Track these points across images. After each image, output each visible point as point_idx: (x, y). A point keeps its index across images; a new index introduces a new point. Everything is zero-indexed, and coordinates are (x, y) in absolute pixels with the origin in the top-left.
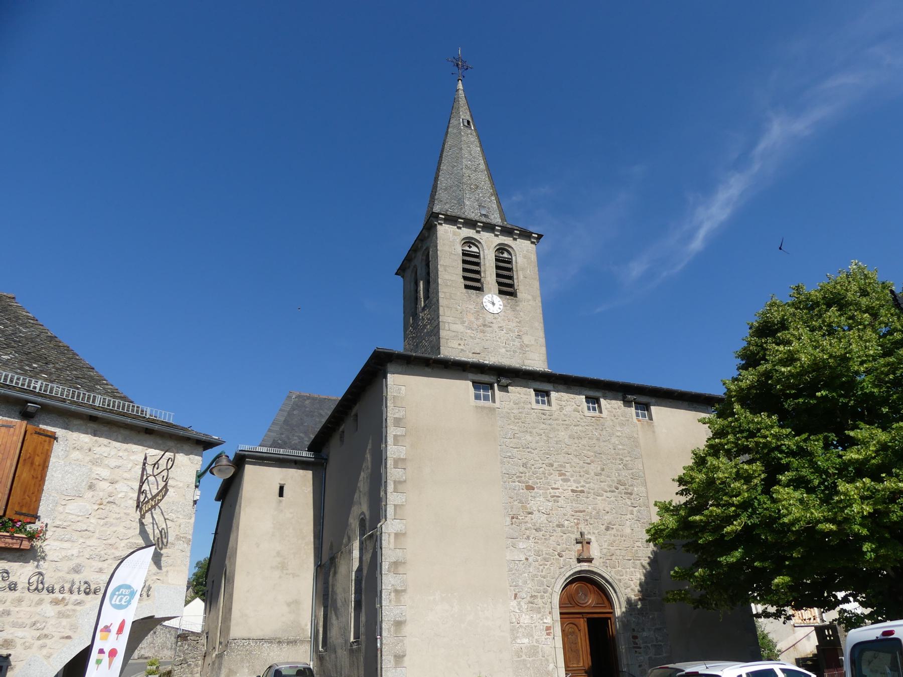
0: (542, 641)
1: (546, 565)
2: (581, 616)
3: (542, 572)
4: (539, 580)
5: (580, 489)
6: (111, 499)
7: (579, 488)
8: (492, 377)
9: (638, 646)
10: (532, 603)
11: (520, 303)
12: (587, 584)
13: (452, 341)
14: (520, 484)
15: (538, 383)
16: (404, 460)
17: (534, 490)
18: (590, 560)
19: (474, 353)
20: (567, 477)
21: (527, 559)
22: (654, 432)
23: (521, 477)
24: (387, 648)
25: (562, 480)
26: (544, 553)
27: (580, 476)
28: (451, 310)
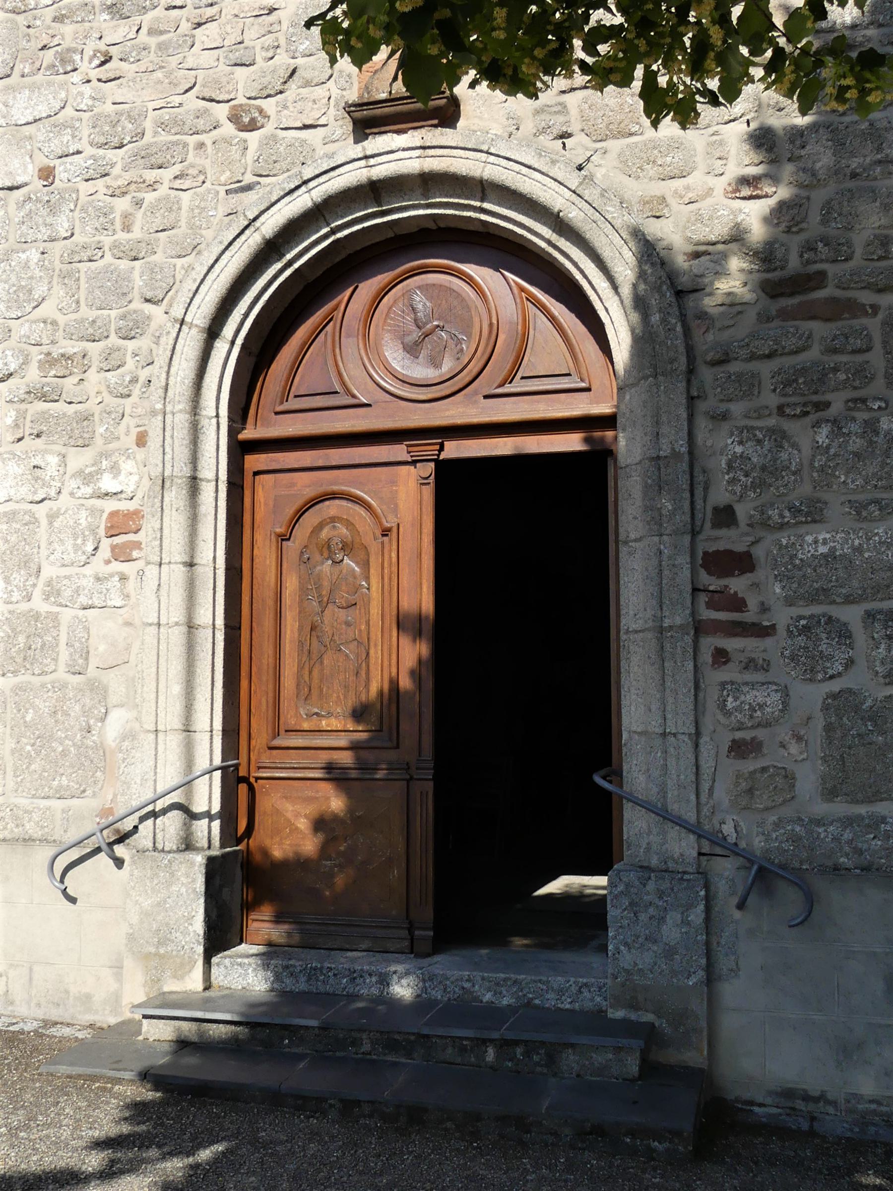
0: (77, 591)
1: (152, 186)
2: (399, 452)
3: (127, 228)
4: (107, 269)
9: (750, 616)
10: (44, 397)
12: (468, 269)
21: (47, 174)
26: (148, 124)
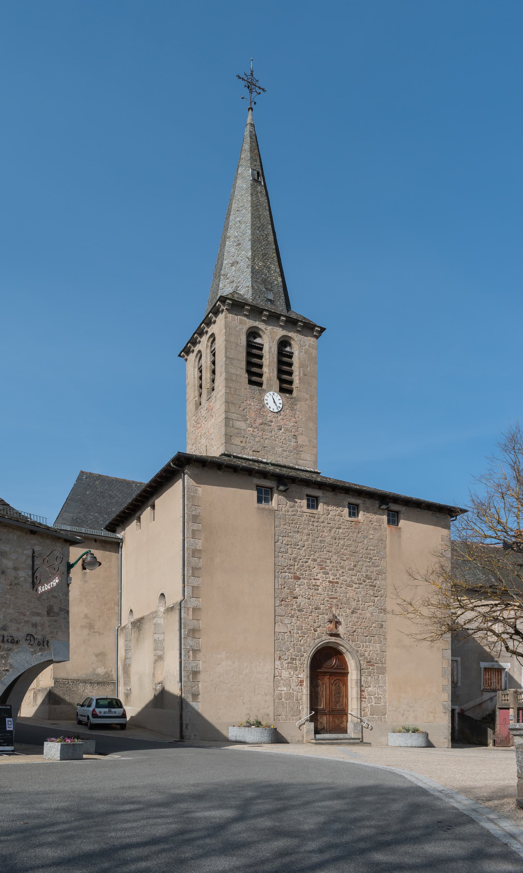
5: (335, 580)
6: (17, 582)
7: (335, 580)
9: (364, 697)
11: (299, 403)
13: (235, 438)
14: (289, 574)
15: (310, 489)
16: (200, 551)
17: (300, 579)
18: (337, 635)
19: (254, 451)
20: (326, 571)
22: (400, 536)
23: (291, 569)
24: (186, 688)
25: (322, 572)
26: (303, 628)
27: (337, 570)
28: (235, 406)
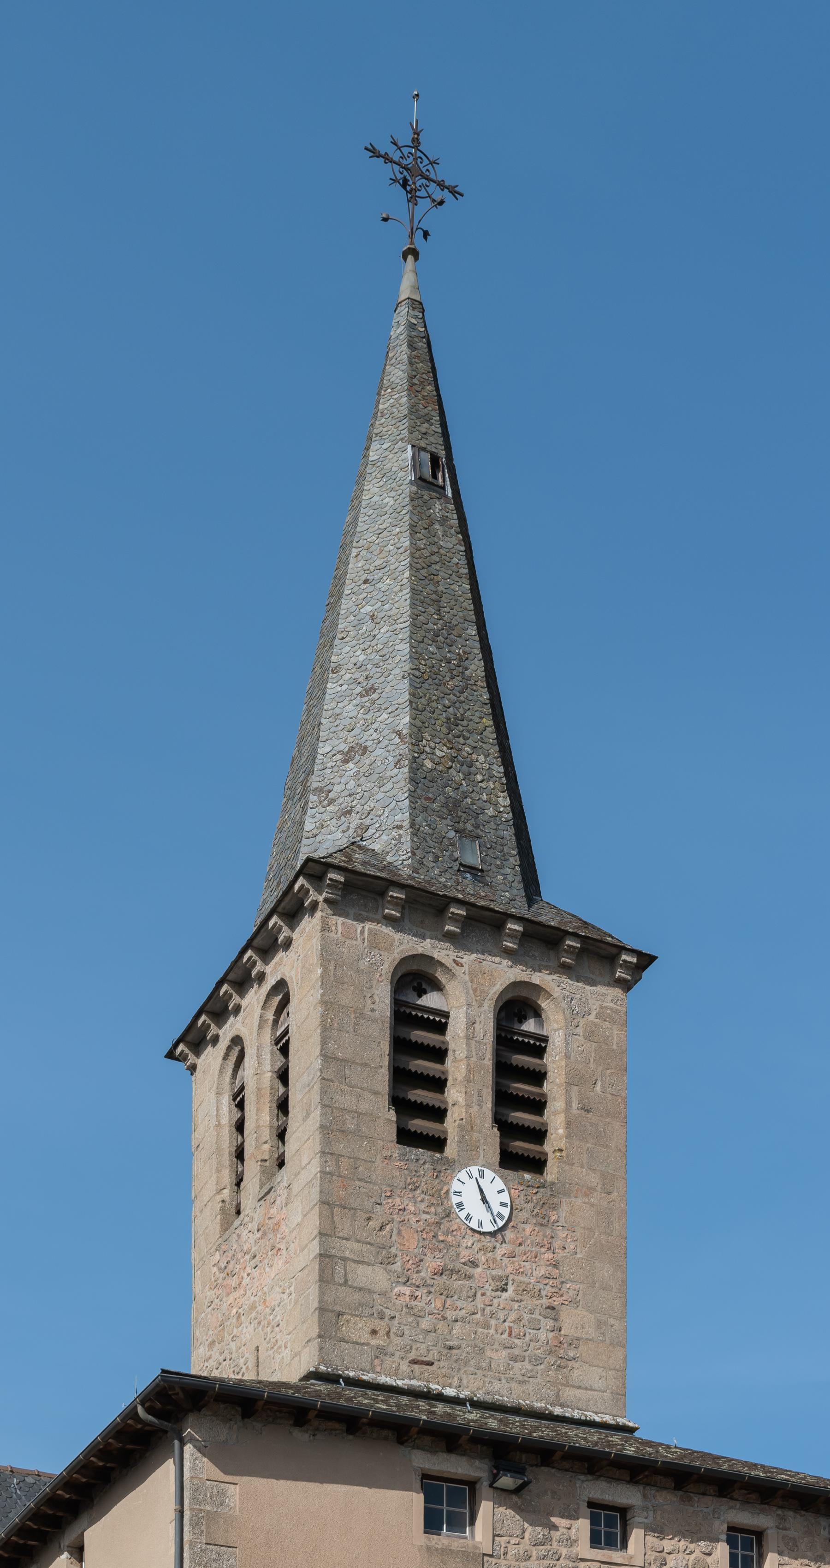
8: (477, 1463)
11: (564, 1200)
15: (603, 1484)
19: (414, 1362)
